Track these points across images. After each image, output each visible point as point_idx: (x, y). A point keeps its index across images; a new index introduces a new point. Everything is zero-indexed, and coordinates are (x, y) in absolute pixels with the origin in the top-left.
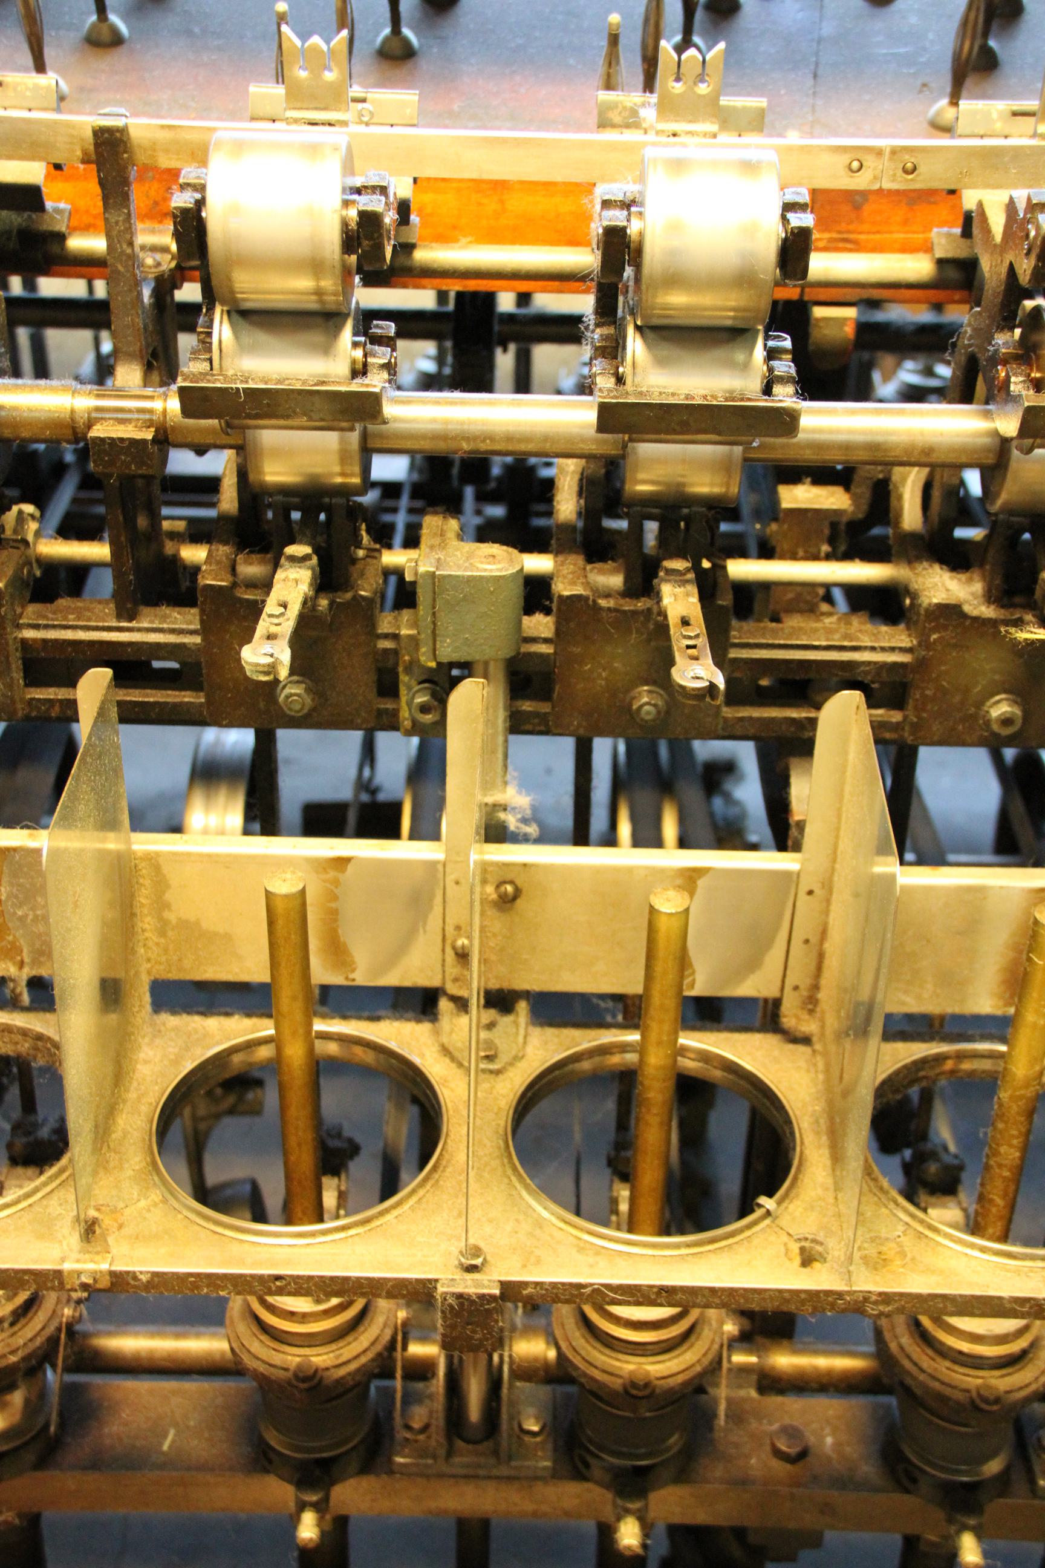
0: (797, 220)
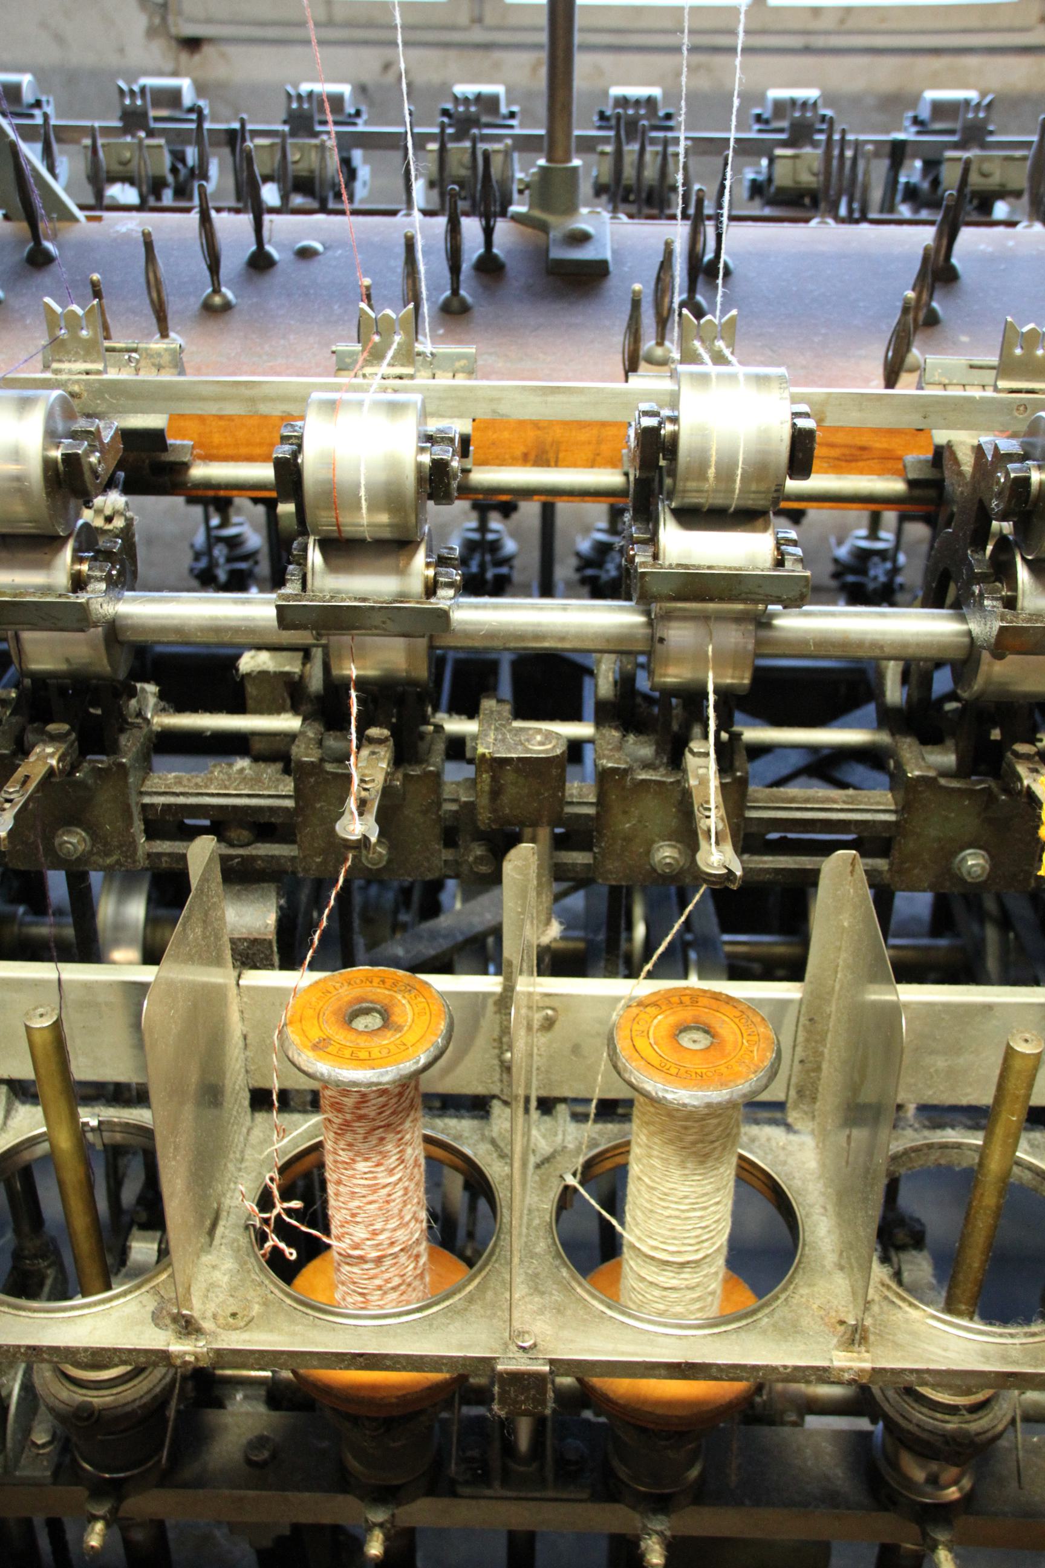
0: (802, 423)
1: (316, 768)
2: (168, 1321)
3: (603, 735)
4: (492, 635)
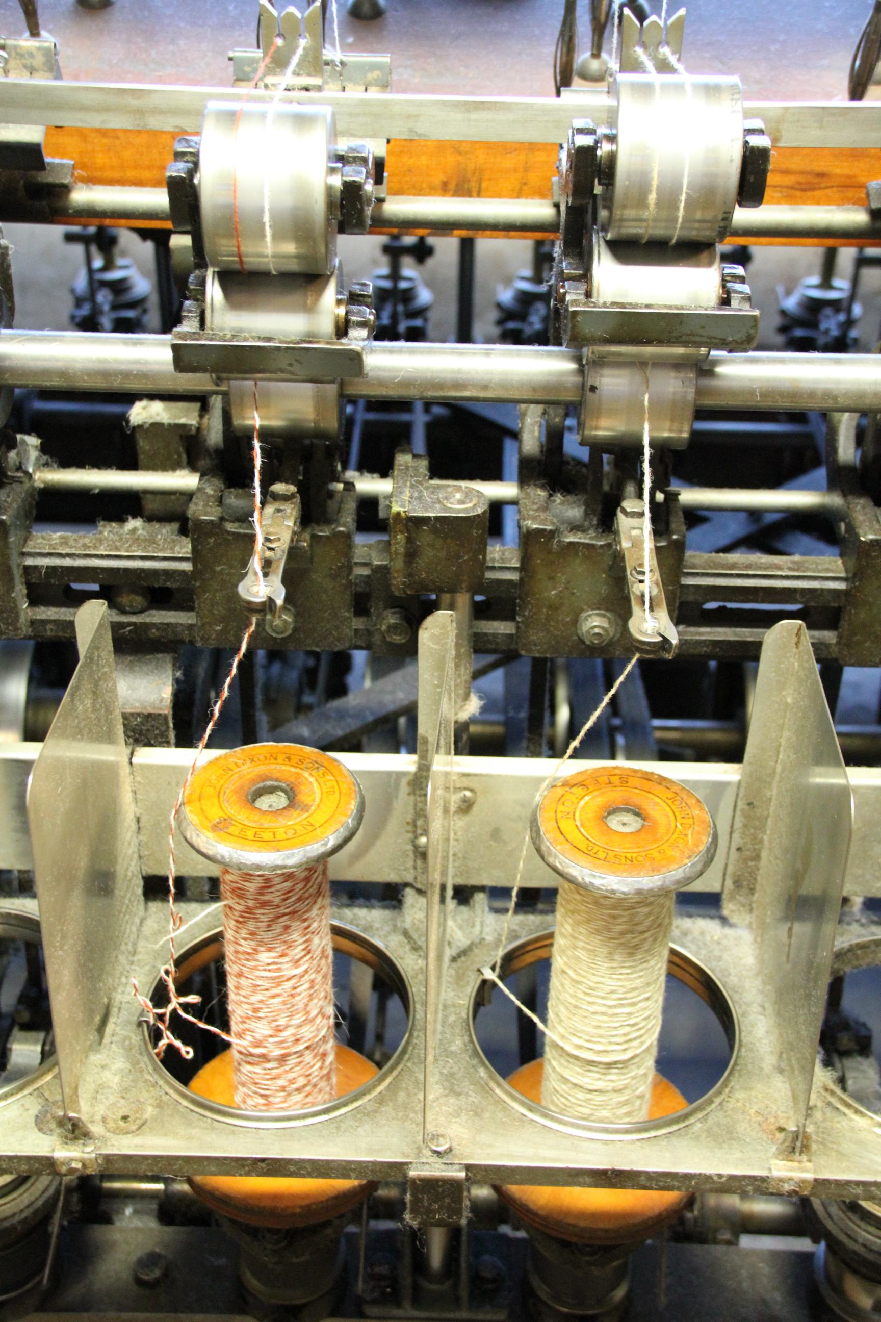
0: (756, 141)
1: (215, 528)
2: (53, 1125)
3: (527, 494)
4: (407, 383)
